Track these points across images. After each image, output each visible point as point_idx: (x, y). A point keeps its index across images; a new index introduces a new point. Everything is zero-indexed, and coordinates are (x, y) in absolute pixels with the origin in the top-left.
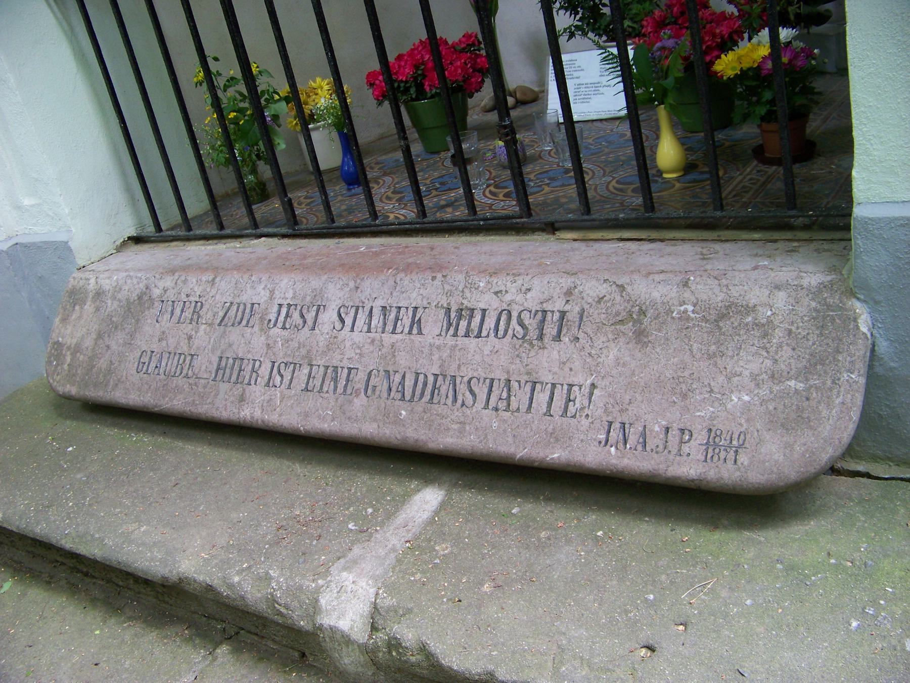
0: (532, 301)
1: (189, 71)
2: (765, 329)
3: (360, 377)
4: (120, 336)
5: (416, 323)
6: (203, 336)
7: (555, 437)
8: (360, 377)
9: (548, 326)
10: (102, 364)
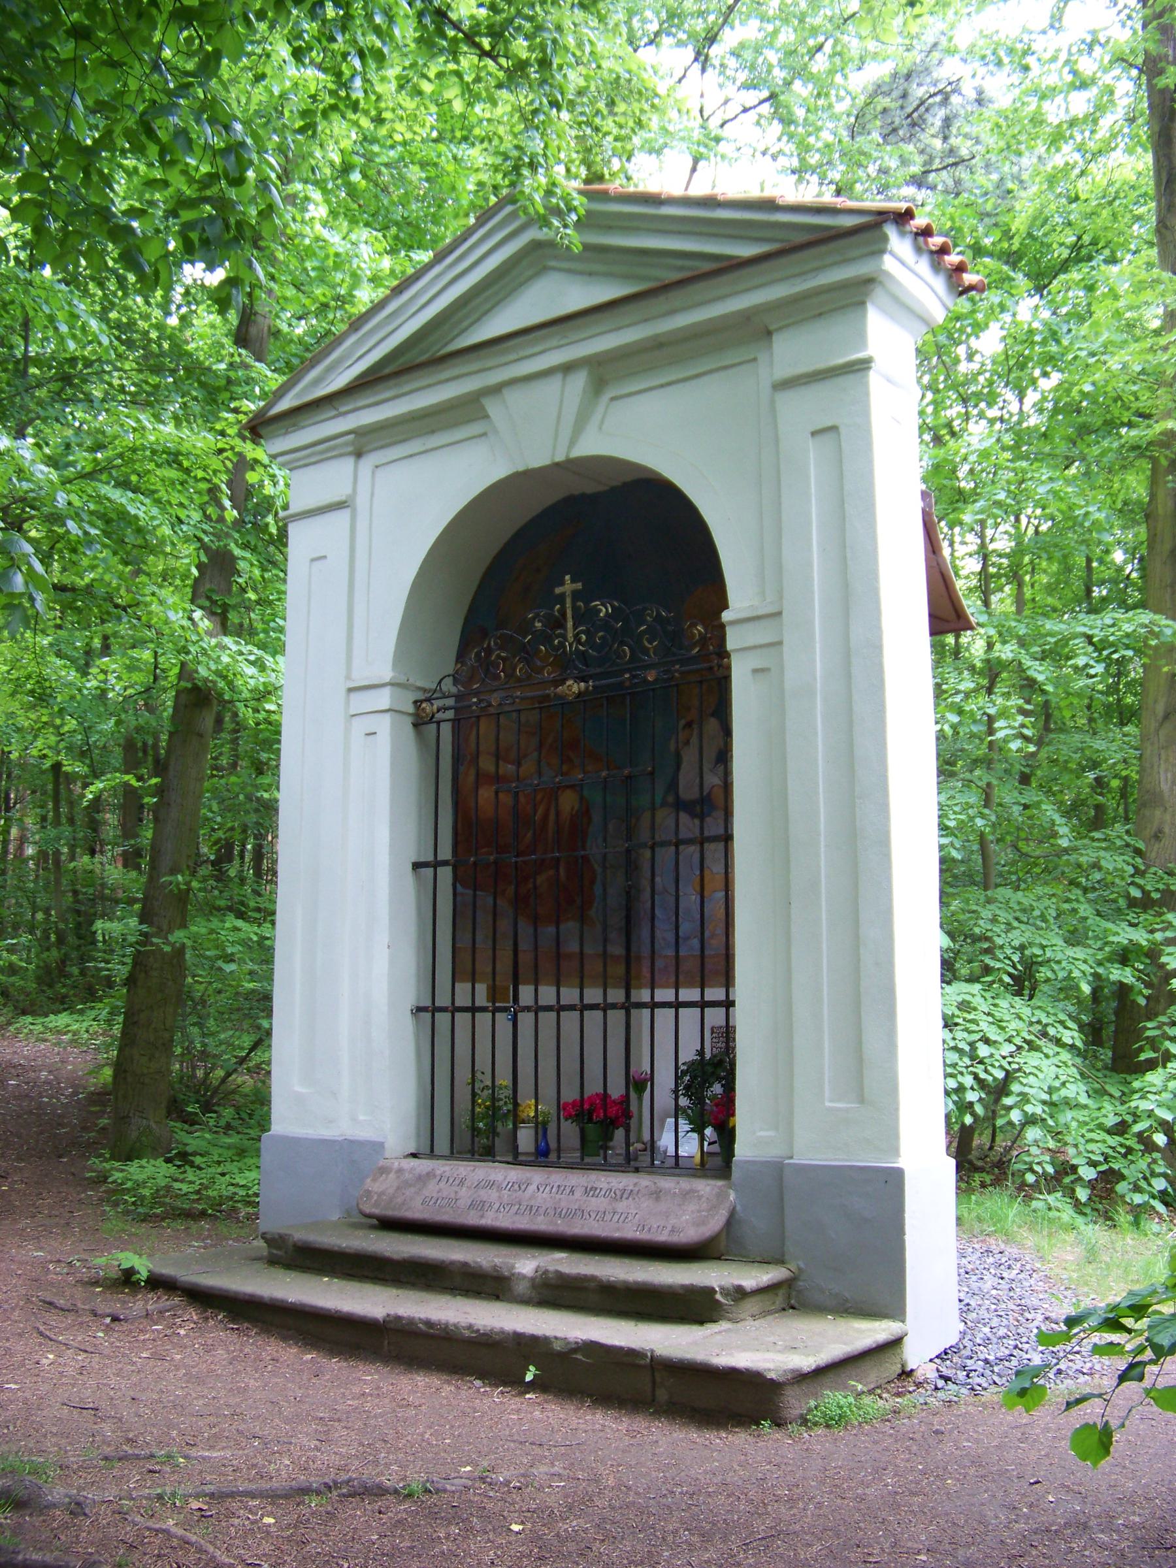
0: (621, 1186)
1: (463, 1074)
2: (700, 1197)
3: (542, 1211)
4: (413, 1190)
5: (572, 1192)
6: (463, 1192)
7: (618, 1229)
8: (542, 1211)
9: (623, 1194)
10: (399, 1200)
